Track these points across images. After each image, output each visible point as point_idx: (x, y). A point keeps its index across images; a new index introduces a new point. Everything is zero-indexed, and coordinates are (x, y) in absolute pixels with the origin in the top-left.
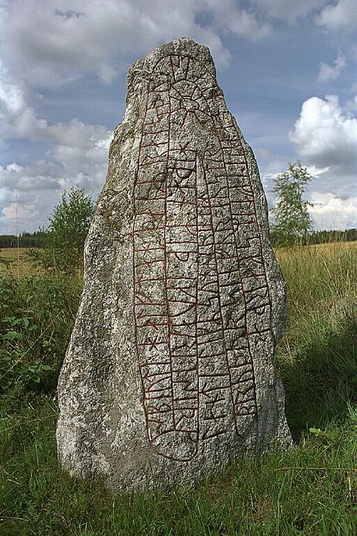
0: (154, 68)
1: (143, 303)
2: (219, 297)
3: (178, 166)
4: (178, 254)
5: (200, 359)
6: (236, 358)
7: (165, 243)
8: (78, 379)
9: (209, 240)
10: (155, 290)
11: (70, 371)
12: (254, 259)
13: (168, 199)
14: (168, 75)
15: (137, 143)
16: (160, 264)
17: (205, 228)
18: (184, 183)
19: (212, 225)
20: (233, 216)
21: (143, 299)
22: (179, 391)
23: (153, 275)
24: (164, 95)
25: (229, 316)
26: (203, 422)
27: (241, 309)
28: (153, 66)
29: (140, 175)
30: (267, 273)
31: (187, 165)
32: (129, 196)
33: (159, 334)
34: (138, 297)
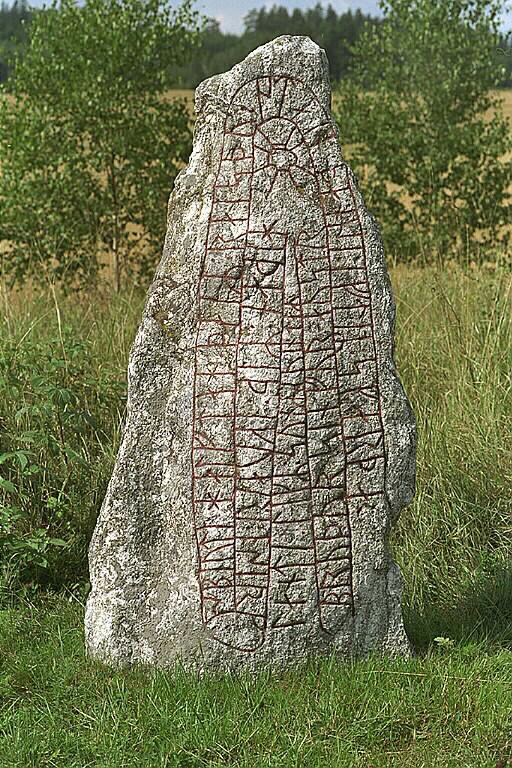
0: (233, 97)
1: (203, 447)
2: (306, 443)
3: (259, 257)
4: (253, 384)
5: (274, 525)
6: (325, 527)
7: (237, 367)
8: (116, 543)
9: (298, 364)
10: (219, 431)
11: (106, 532)
12: (365, 391)
13: (243, 304)
14: (252, 111)
15: (206, 211)
16: (228, 395)
17: (293, 348)
18: (266, 281)
19: (302, 344)
20: (336, 330)
21: (204, 441)
22: (243, 563)
23: (219, 410)
24: (246, 141)
25: (320, 470)
26: (272, 606)
27: (339, 461)
28: (232, 94)
29: (208, 263)
30: (383, 412)
31: (271, 256)
32: (192, 292)
33: (223, 488)
34: (197, 439)
